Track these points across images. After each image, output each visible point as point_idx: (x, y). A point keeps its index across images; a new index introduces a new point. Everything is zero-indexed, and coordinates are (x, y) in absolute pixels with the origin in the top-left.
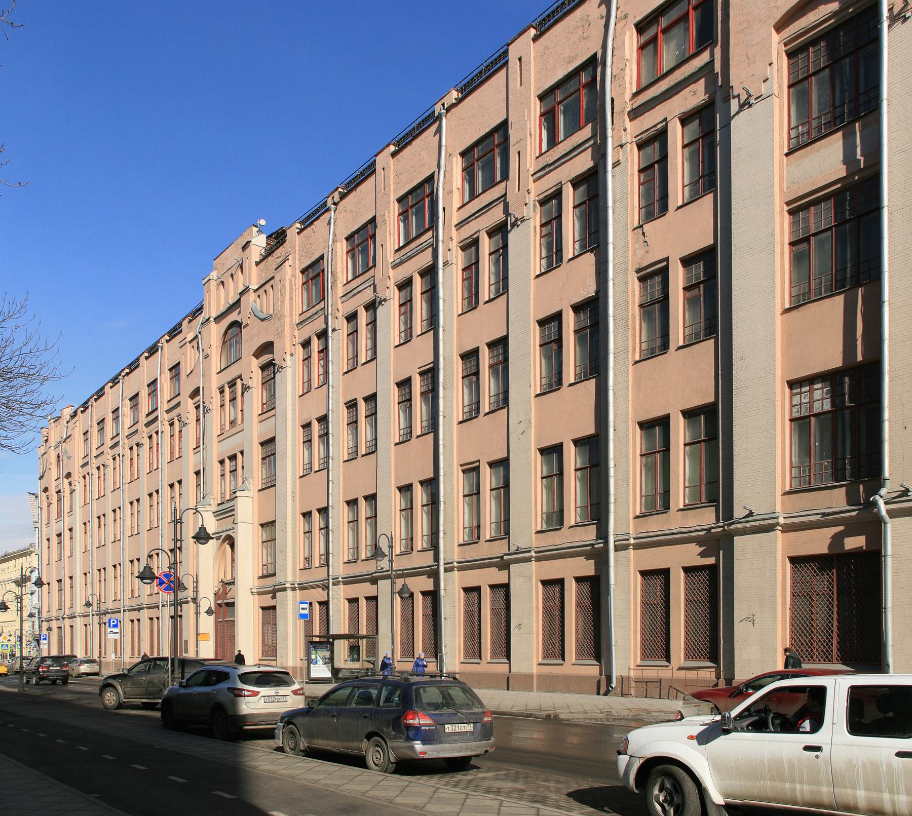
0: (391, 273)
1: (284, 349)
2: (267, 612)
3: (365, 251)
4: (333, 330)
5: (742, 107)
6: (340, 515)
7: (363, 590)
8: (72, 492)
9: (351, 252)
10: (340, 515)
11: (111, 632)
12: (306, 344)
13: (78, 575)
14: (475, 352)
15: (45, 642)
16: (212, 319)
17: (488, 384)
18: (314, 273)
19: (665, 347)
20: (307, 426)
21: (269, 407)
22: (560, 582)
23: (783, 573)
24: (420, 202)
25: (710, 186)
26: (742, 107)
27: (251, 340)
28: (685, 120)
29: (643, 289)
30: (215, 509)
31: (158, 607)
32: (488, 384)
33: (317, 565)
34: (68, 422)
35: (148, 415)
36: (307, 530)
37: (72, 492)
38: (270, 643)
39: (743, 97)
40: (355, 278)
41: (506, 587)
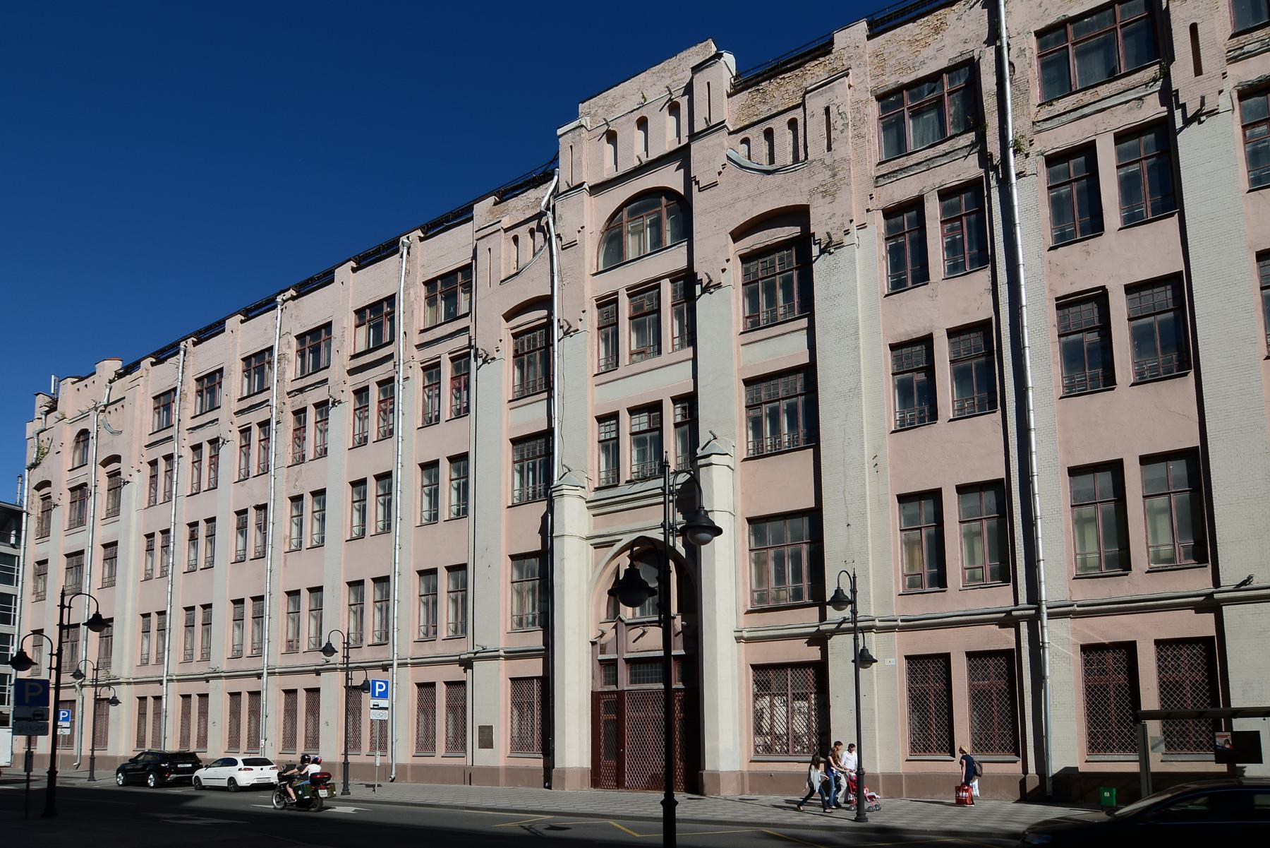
0: (287, 400)
1: (849, 214)
2: (424, 690)
3: (316, 351)
4: (1019, 175)
5: (822, 252)
6: (276, 607)
7: (194, 689)
8: (47, 512)
9: (200, 393)
10: (276, 607)
11: (376, 707)
12: (154, 464)
13: (129, 616)
14: (196, 524)
15: (67, 724)
16: (585, 186)
17: (375, 511)
18: (164, 401)
19: (362, 535)
20: (150, 536)
21: (114, 511)
22: (432, 685)
23: (505, 689)
24: (315, 341)
25: (984, 258)
26: (822, 252)
27: (97, 451)
28: (944, 194)
29: (952, 345)
30: (592, 496)
31: (161, 682)
32: (375, 511)
33: (249, 653)
34: (111, 382)
35: (354, 357)
36: (291, 610)
37: (47, 512)
38: (780, 729)
39: (705, 282)
40: (201, 414)
41: (317, 690)
